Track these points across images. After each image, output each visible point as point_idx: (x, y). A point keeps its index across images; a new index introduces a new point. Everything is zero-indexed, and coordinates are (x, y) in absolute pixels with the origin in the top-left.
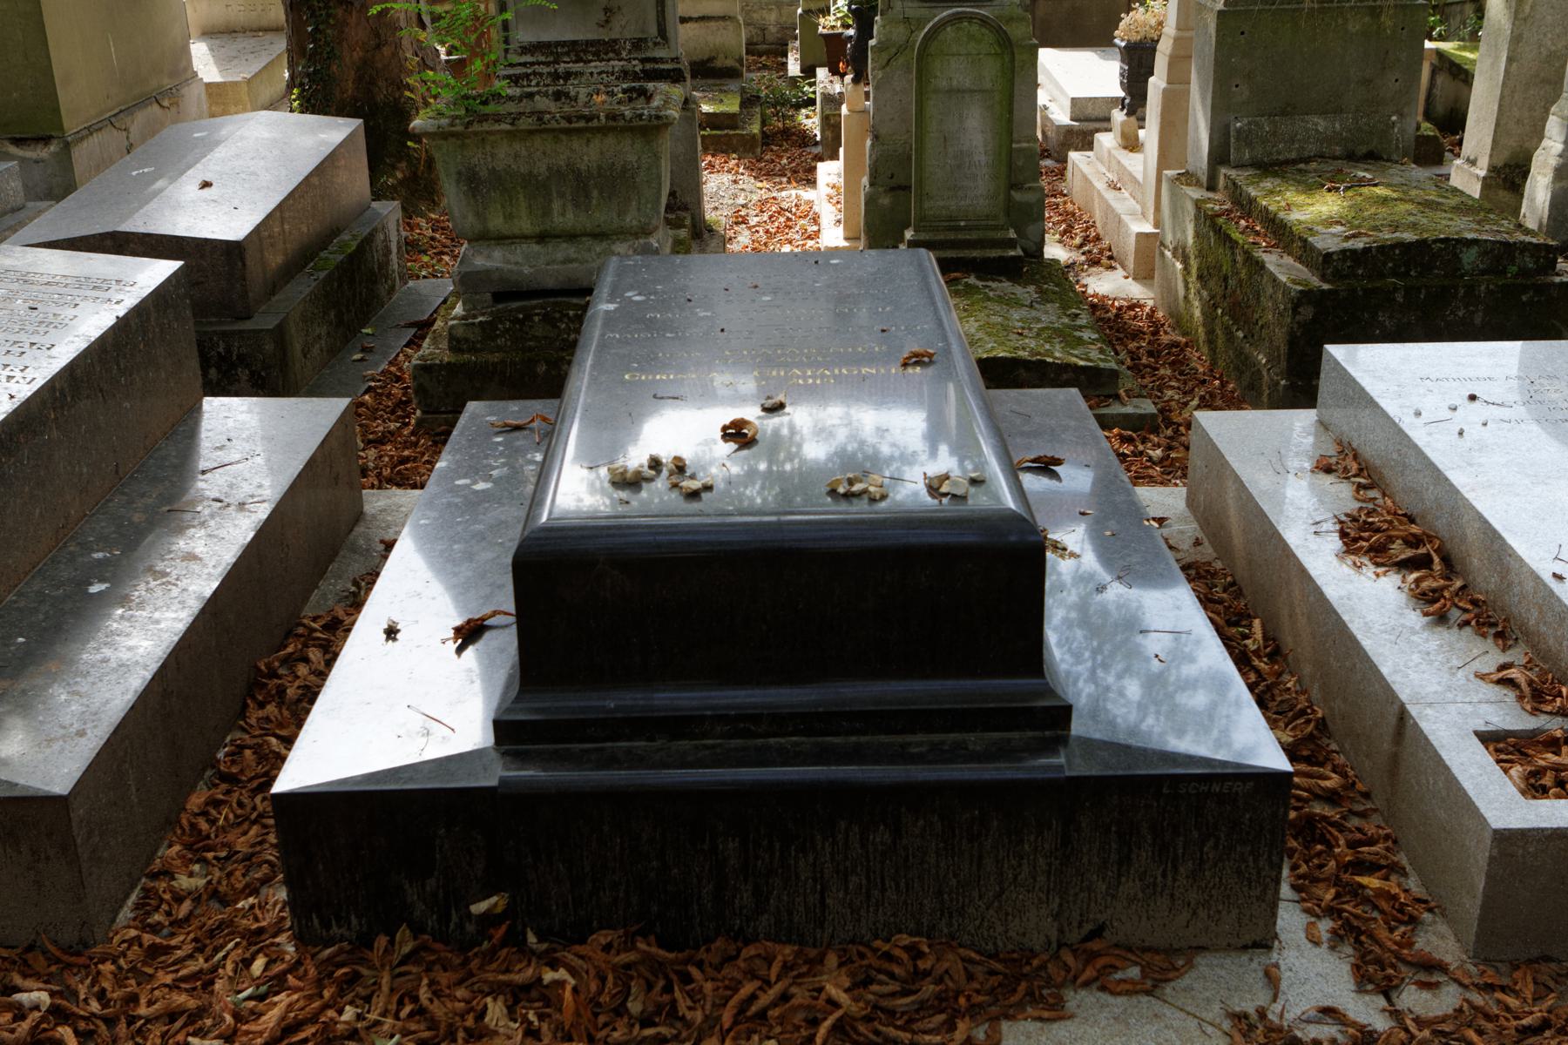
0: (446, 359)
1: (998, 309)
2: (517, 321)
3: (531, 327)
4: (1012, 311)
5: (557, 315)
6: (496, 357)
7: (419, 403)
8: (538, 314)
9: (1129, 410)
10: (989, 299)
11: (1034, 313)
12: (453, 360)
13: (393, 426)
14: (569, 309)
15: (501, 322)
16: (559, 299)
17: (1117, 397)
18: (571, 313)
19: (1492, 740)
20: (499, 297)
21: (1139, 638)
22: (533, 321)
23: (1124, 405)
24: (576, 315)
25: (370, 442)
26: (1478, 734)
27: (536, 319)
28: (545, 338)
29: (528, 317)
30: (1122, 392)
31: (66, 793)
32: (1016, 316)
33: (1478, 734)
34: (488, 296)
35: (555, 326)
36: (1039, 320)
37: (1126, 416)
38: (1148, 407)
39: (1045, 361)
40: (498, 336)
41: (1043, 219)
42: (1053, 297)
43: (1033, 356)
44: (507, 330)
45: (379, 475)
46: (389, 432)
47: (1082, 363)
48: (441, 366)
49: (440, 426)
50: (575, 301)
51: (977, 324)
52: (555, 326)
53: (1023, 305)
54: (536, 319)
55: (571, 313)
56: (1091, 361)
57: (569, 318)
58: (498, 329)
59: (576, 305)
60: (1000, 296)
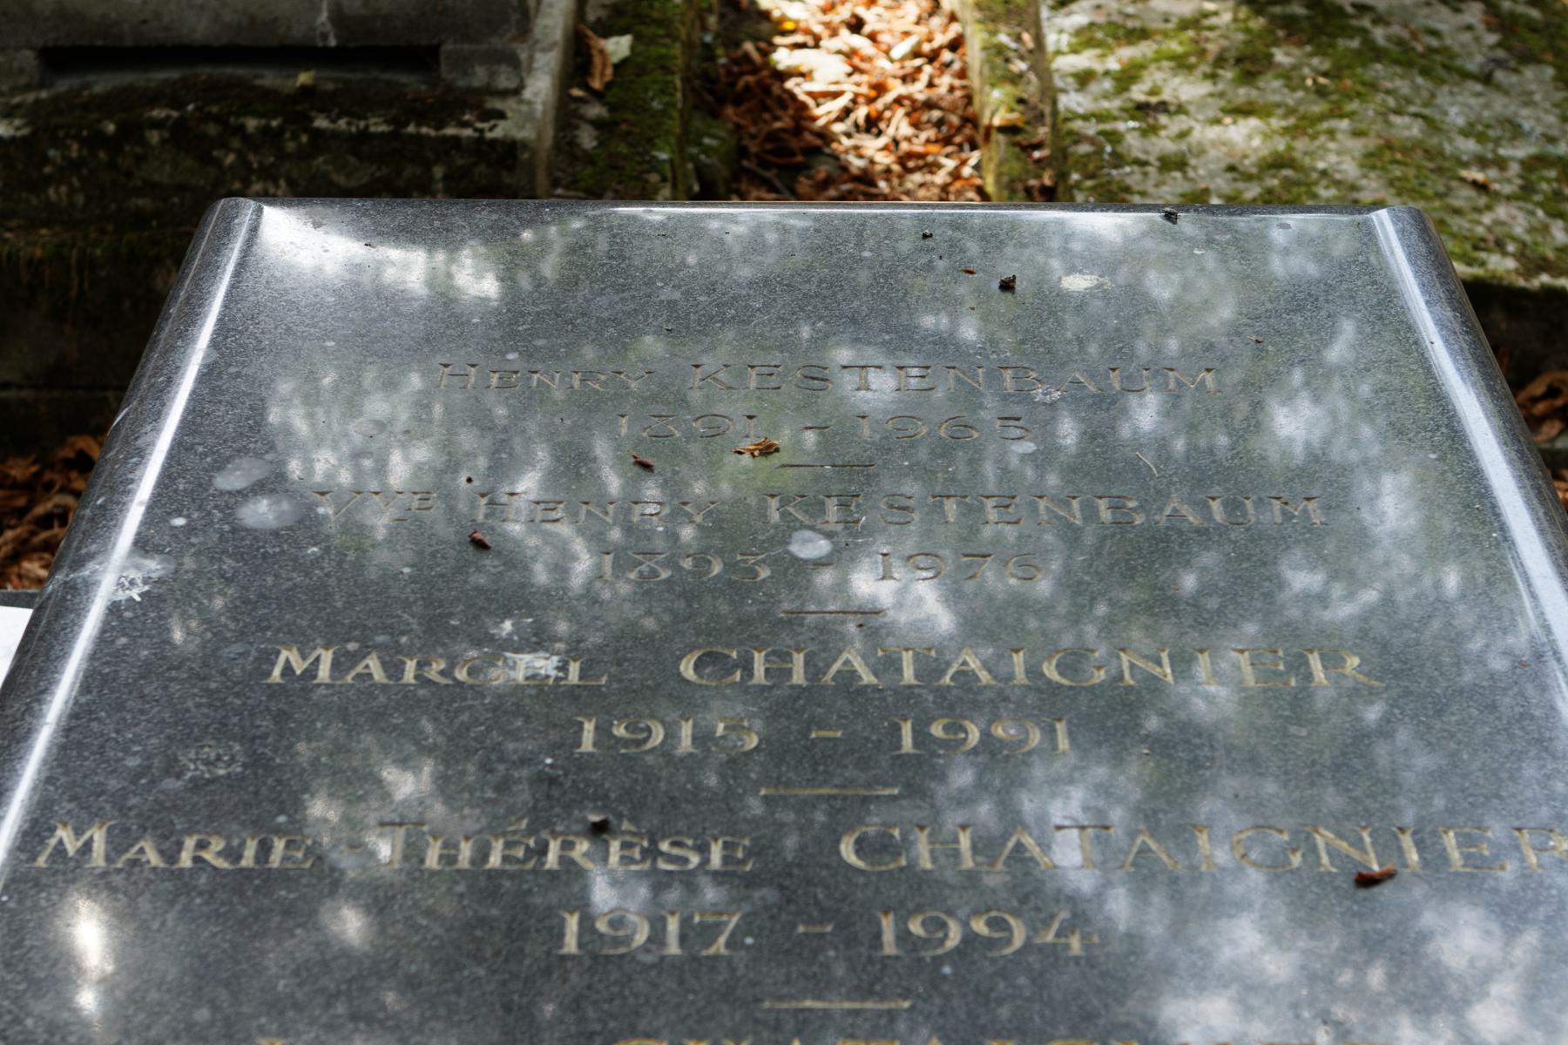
1: (1404, 87)
2: (97, 140)
3: (140, 159)
4: (1443, 98)
5: (212, 129)
6: (39, 244)
8: (158, 125)
10: (1378, 54)
11: (1500, 105)
14: (248, 110)
15: (57, 143)
16: (229, 70)
18: (252, 124)
20: (57, 59)
22: (143, 142)
24: (265, 131)
26: (777, 450)
27: (154, 137)
28: (181, 188)
29: (132, 131)
32: (1456, 116)
33: (777, 450)
34: (28, 57)
35: (206, 159)
36: (1516, 132)
40: (48, 180)
41: (826, 136)
42: (1536, 42)
44: (75, 166)
50: (269, 79)
51: (1358, 146)
52: (206, 159)
53: (1466, 75)
54: (154, 137)
55: (252, 124)
57: (246, 138)
58: (46, 160)
59: (268, 94)
60: (1400, 42)
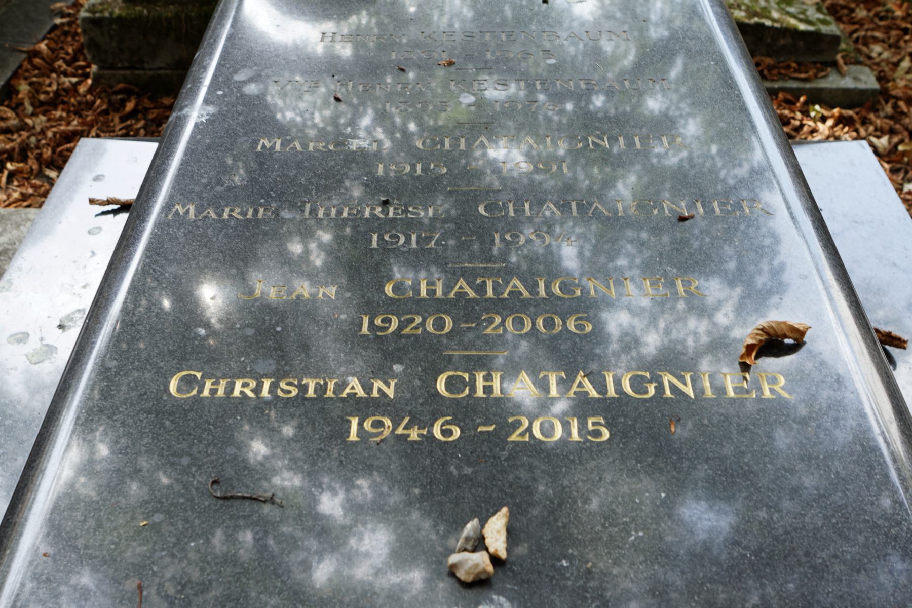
0: (117, 11)
7: (94, 58)
9: (847, 83)
12: (124, 14)
13: (67, 81)
17: (834, 64)
19: (466, 560)
21: (50, 551)
23: (842, 74)
25: (42, 104)
30: (839, 57)
31: (86, 145)
37: (846, 91)
38: (868, 81)
39: (762, 26)
43: (750, 17)
45: (39, 157)
46: (64, 90)
47: (802, 27)
48: (112, 20)
49: (119, 82)
56: (807, 21)
